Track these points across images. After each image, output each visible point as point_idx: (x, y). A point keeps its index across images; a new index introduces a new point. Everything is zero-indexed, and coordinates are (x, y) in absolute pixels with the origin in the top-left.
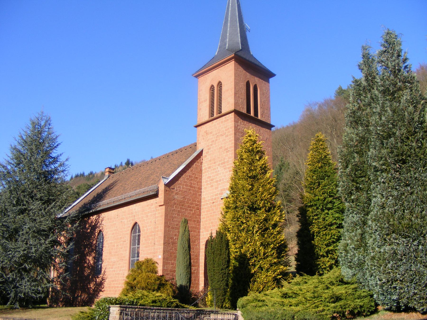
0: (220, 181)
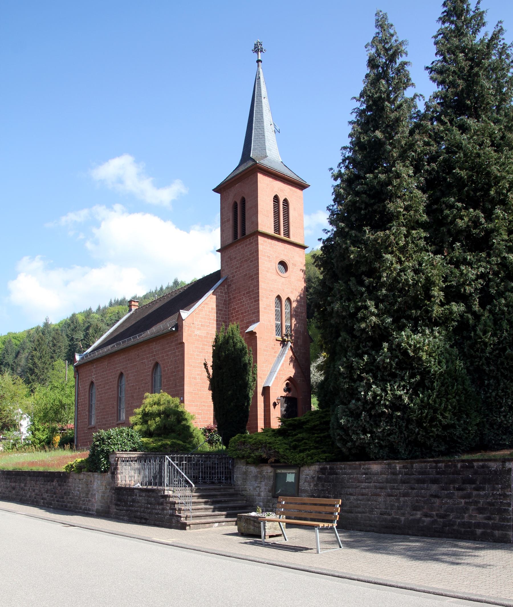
0: (246, 312)
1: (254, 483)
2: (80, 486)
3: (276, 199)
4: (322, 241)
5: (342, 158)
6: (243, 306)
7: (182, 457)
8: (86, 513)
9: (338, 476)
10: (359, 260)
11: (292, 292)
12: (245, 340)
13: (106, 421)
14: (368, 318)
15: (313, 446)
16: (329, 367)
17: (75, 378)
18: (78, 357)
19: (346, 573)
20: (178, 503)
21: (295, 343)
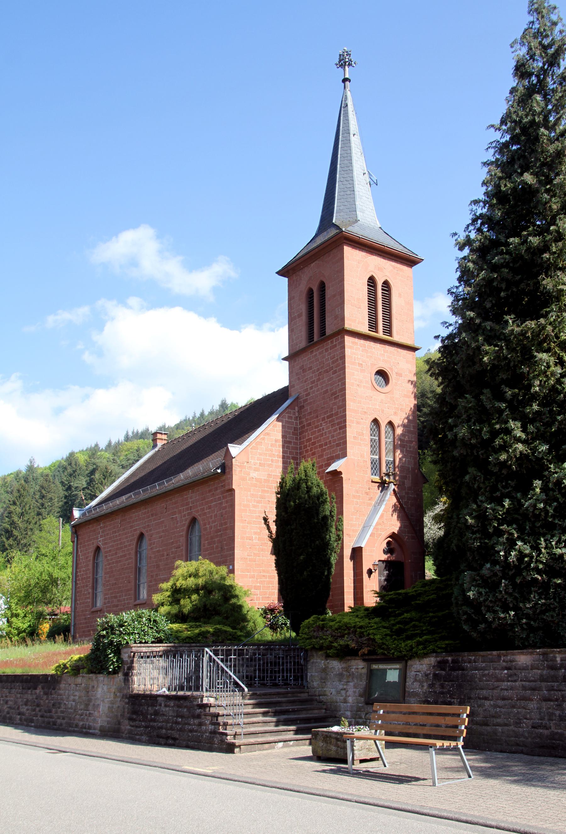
1: (338, 684)
2: (77, 693)
3: (372, 281)
4: (440, 339)
5: (471, 217)
6: (322, 435)
7: (230, 650)
8: (85, 732)
9: (466, 672)
10: (496, 362)
11: (395, 413)
12: (325, 483)
13: (119, 601)
14: (511, 446)
15: (427, 629)
16: (451, 518)
17: (73, 542)
18: (77, 513)
19: (479, 816)
20: (223, 715)
21: (400, 485)
